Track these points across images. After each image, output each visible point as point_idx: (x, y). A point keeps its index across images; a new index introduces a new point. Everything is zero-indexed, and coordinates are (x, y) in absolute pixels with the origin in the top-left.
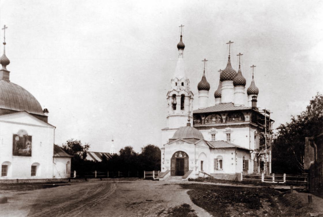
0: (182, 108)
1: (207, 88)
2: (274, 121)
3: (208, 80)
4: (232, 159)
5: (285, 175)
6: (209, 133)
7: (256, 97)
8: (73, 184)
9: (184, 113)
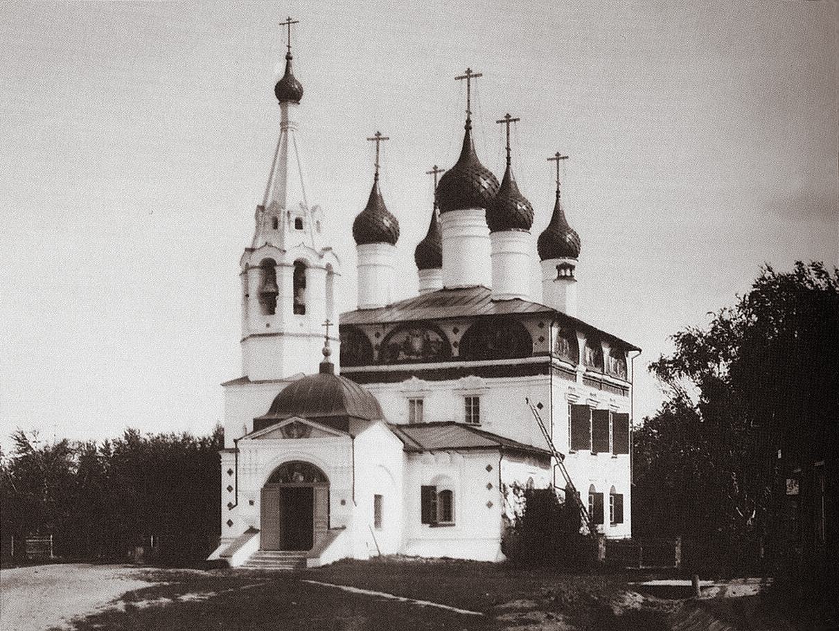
0: (300, 309)
1: (390, 236)
2: (640, 351)
3: (392, 202)
4: (490, 486)
5: (679, 542)
6: (402, 394)
7: (572, 268)
8: (397, 316)
9: (272, 325)
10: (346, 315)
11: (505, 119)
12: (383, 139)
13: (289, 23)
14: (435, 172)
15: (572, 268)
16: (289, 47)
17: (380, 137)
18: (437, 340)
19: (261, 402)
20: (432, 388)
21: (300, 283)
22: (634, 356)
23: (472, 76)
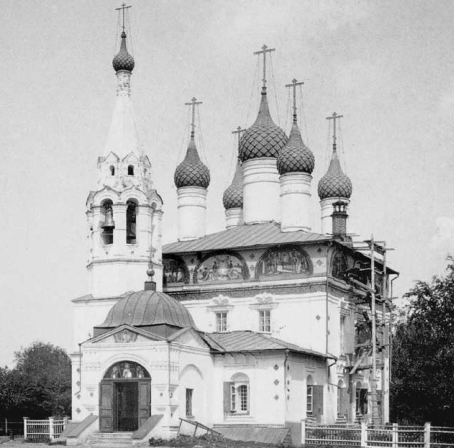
0: (131, 238)
2: (398, 274)
3: (206, 157)
7: (345, 205)
10: (168, 246)
11: (292, 83)
12: (198, 103)
13: (124, 8)
14: (239, 132)
15: (345, 205)
16: (124, 27)
17: (196, 101)
18: (238, 264)
19: (100, 314)
20: (234, 304)
21: (131, 220)
22: (393, 278)
23: (268, 51)
